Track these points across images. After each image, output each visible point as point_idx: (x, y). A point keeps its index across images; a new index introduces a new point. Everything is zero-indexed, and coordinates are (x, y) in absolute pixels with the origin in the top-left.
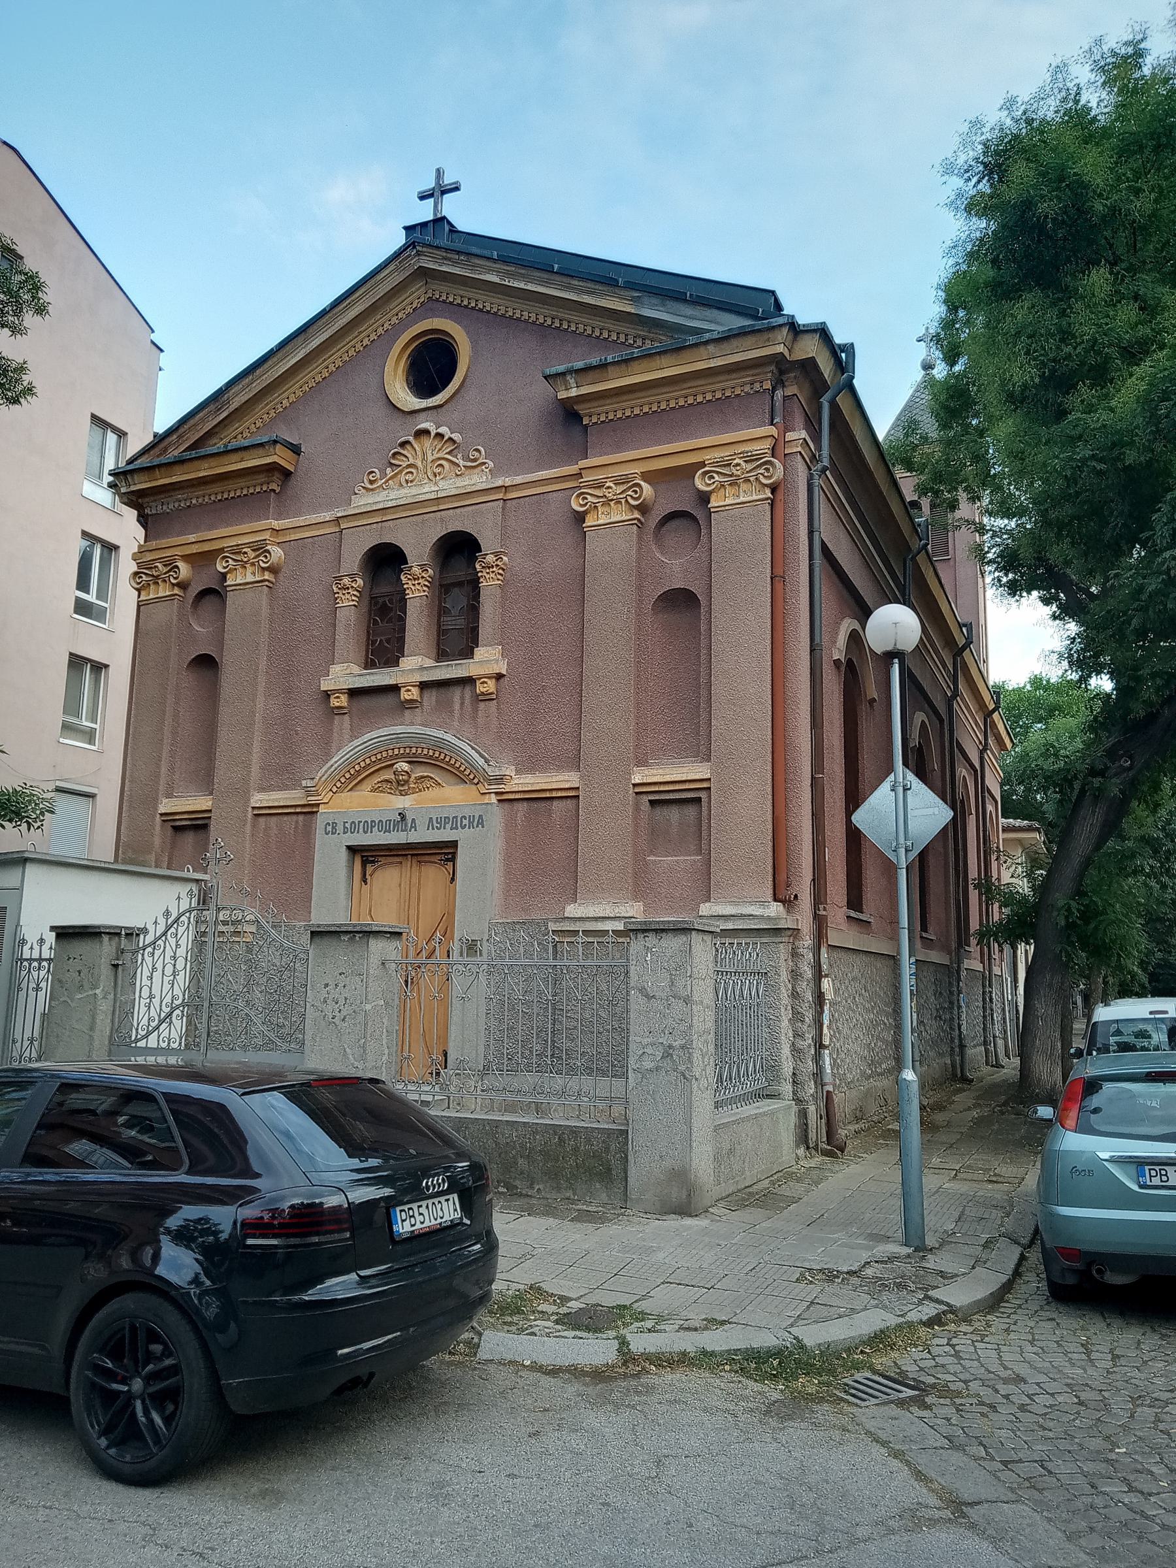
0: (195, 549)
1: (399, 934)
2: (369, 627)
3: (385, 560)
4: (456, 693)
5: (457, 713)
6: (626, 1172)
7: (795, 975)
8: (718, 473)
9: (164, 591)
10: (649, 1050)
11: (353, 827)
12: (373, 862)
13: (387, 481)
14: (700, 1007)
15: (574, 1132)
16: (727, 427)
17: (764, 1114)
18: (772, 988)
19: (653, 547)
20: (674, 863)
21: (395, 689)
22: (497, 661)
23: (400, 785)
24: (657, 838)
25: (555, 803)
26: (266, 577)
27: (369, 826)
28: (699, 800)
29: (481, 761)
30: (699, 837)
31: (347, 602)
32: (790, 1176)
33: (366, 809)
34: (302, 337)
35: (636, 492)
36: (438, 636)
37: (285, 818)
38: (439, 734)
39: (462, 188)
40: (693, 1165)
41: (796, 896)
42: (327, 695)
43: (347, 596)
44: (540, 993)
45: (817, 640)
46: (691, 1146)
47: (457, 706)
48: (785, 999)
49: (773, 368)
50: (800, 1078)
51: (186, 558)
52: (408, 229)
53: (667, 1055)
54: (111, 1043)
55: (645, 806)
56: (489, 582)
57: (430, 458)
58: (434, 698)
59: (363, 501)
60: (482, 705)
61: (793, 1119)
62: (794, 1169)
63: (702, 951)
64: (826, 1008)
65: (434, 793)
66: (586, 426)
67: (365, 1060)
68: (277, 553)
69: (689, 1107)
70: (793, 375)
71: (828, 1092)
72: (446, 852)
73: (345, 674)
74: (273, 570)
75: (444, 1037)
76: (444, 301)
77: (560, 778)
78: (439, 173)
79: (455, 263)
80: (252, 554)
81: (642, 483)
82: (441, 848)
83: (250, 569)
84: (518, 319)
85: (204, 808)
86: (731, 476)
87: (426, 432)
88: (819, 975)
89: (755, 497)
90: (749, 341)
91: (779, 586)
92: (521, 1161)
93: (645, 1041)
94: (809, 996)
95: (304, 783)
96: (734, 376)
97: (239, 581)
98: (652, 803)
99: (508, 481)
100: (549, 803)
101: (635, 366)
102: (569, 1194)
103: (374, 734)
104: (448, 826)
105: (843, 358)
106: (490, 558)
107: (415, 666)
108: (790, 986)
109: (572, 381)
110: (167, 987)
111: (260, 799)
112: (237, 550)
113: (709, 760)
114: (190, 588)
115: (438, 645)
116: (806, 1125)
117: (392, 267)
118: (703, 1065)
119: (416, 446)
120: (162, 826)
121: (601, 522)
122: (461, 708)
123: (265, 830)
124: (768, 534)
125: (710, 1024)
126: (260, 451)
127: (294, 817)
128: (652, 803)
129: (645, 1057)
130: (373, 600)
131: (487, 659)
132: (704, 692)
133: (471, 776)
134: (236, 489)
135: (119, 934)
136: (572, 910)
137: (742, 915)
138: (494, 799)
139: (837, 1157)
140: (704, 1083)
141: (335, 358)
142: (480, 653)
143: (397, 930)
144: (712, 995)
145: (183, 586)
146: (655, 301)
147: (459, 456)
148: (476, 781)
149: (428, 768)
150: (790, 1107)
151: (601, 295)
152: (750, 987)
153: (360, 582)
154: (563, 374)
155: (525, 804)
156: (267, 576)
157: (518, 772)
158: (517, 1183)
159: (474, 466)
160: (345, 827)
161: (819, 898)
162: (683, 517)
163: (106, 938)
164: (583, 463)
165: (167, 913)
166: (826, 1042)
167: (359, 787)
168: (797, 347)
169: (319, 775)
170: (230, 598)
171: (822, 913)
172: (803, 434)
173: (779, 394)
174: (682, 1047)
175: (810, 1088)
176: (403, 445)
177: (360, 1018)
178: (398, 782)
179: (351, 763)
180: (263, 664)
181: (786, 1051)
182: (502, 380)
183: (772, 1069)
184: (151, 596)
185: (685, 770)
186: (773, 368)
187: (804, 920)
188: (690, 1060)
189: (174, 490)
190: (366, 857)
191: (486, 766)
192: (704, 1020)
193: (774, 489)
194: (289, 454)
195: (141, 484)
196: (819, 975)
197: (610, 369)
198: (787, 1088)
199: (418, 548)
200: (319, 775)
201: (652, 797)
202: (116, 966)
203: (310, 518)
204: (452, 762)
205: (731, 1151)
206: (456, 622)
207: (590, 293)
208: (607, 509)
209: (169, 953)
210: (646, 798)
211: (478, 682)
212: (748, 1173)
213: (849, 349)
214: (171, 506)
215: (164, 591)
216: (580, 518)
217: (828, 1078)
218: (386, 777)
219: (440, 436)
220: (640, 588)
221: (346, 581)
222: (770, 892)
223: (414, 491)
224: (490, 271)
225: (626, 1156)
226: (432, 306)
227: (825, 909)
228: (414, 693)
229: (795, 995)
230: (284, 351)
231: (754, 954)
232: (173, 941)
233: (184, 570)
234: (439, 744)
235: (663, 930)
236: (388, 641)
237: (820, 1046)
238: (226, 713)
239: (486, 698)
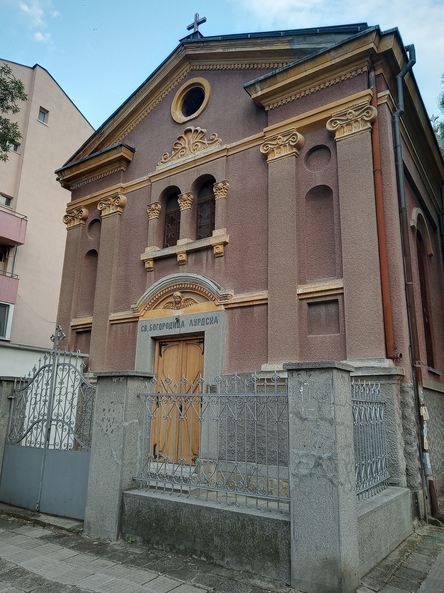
0: (89, 202)
1: (149, 378)
2: (165, 228)
3: (171, 195)
4: (204, 255)
5: (204, 266)
6: (289, 555)
7: (403, 404)
8: (339, 120)
9: (76, 222)
10: (304, 460)
11: (154, 328)
12: (164, 345)
13: (172, 157)
14: (342, 427)
15: (252, 519)
16: (343, 95)
17: (392, 501)
18: (389, 413)
19: (305, 166)
20: (323, 339)
21: (174, 256)
22: (223, 235)
23: (177, 304)
24: (312, 325)
25: (255, 308)
26: (118, 210)
27: (162, 326)
28: (336, 301)
29: (216, 288)
30: (338, 323)
31: (154, 216)
32: (412, 546)
33: (159, 318)
34: (134, 98)
35: (294, 138)
36: (197, 229)
37: (125, 325)
38: (195, 275)
39: (207, 20)
40: (343, 555)
41: (401, 355)
42: (144, 262)
43: (154, 214)
44: (248, 415)
45: (403, 206)
46: (339, 540)
47: (204, 261)
48: (399, 421)
49: (368, 58)
50: (411, 471)
51: (86, 206)
52: (180, 41)
53: (318, 465)
54: (6, 443)
55: (305, 306)
56: (220, 197)
57: (192, 142)
58: (193, 259)
59: (161, 168)
60: (217, 260)
61: (409, 501)
62: (412, 538)
63: (342, 386)
64: (425, 426)
65: (193, 307)
66: (267, 111)
67: (123, 459)
68: (123, 198)
69: (337, 508)
70: (379, 63)
71: (431, 482)
72: (198, 338)
73: (152, 251)
74: (122, 206)
75: (197, 441)
76: (198, 70)
77: (257, 294)
78: (197, 16)
79: (202, 48)
80: (112, 200)
81: (297, 133)
82: (197, 336)
83: (111, 207)
84: (233, 69)
85: (89, 322)
86: (347, 120)
87: (190, 131)
88: (418, 405)
89: (361, 129)
90: (354, 45)
91: (378, 175)
92: (216, 539)
93: (301, 452)
94: (413, 418)
95: (132, 306)
96: (345, 68)
97: (107, 214)
98: (310, 305)
99: (229, 146)
100: (252, 308)
101: (291, 72)
102: (249, 568)
103: (164, 279)
104: (200, 324)
105: (408, 54)
106: (220, 185)
107: (184, 243)
108: (400, 412)
109: (258, 87)
110: (32, 411)
111: (113, 316)
112: (106, 199)
113: (342, 277)
114: (88, 220)
115: (197, 233)
116: (417, 503)
117: (173, 57)
118: (346, 473)
119: (185, 138)
120: (72, 332)
121: (276, 157)
122: (207, 263)
123: (116, 331)
124: (370, 148)
125: (351, 440)
126: (115, 151)
127: (128, 324)
128: (310, 305)
129: (302, 466)
130: (167, 215)
131: (219, 235)
132: (337, 240)
133: (211, 297)
134: (106, 172)
135: (13, 382)
136: (265, 367)
137: (367, 367)
138: (223, 308)
139: (440, 526)
140: (348, 486)
141: (150, 106)
142: (215, 233)
143: (149, 375)
144: (350, 418)
145: (84, 219)
146: (301, 39)
147: (206, 139)
148: (213, 299)
149: (191, 295)
150: (407, 493)
151: (272, 44)
152: (376, 412)
153: (159, 206)
154: (254, 84)
155: (239, 310)
156: (119, 209)
157: (236, 293)
158: (213, 554)
159: (213, 142)
160: (151, 327)
161: (415, 358)
162: (321, 147)
163: (5, 384)
164: (265, 130)
165: (34, 369)
166: (426, 447)
167: (158, 307)
168: (381, 46)
169: (139, 301)
170: (103, 222)
171: (418, 366)
172: (388, 92)
173: (372, 74)
174: (330, 459)
175: (418, 479)
176: (179, 138)
177: (121, 431)
178: (175, 302)
179: (154, 294)
180: (116, 251)
181: (401, 454)
182: (225, 99)
183: (392, 466)
184: (72, 226)
185: (328, 284)
186: (368, 58)
187: (406, 369)
188: (336, 470)
189: (82, 176)
190: (161, 342)
191: (218, 290)
192: (345, 437)
193: (372, 122)
194: (129, 152)
195: (68, 175)
196: (418, 405)
197: (278, 77)
198: (403, 479)
199: (186, 185)
200: (139, 301)
201: (309, 301)
202: (11, 399)
203: (137, 181)
204: (202, 290)
205: (371, 534)
206: (205, 222)
207: (266, 45)
208: (279, 150)
209: (34, 391)
210: (305, 302)
211: (215, 248)
212: (383, 548)
213: (411, 48)
214: (81, 184)
215: (76, 222)
216: (265, 156)
217: (429, 472)
218: (170, 301)
219: (196, 131)
220: (298, 188)
221: (153, 206)
222: (384, 353)
223: (184, 159)
224: (218, 47)
225: (290, 544)
226: (193, 73)
227: (419, 363)
228: (184, 257)
229: (404, 417)
230: (127, 105)
231: (376, 390)
232: (36, 384)
233: (85, 212)
234: (195, 281)
235: (311, 370)
236: (173, 234)
237: (422, 450)
238: (99, 274)
239: (219, 255)
